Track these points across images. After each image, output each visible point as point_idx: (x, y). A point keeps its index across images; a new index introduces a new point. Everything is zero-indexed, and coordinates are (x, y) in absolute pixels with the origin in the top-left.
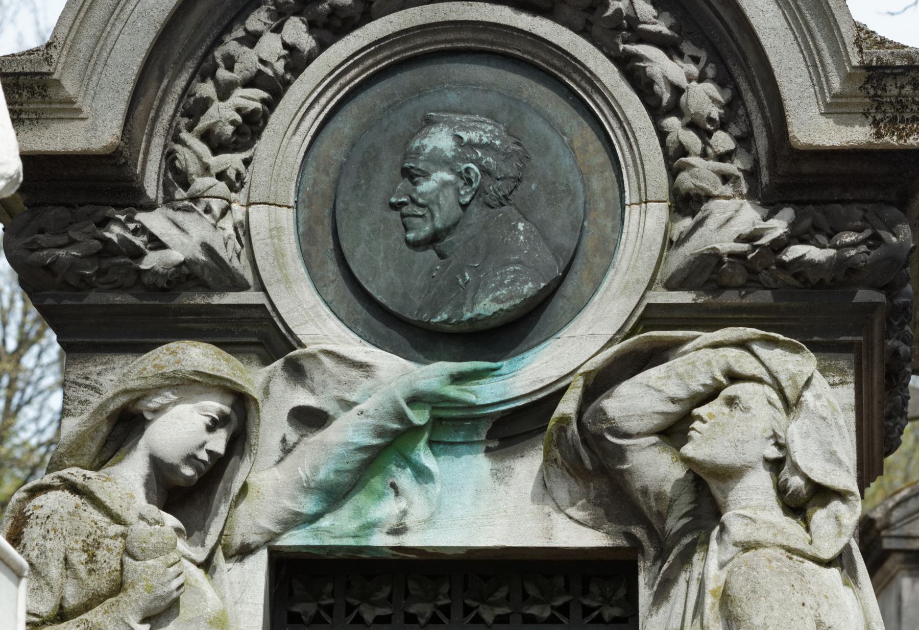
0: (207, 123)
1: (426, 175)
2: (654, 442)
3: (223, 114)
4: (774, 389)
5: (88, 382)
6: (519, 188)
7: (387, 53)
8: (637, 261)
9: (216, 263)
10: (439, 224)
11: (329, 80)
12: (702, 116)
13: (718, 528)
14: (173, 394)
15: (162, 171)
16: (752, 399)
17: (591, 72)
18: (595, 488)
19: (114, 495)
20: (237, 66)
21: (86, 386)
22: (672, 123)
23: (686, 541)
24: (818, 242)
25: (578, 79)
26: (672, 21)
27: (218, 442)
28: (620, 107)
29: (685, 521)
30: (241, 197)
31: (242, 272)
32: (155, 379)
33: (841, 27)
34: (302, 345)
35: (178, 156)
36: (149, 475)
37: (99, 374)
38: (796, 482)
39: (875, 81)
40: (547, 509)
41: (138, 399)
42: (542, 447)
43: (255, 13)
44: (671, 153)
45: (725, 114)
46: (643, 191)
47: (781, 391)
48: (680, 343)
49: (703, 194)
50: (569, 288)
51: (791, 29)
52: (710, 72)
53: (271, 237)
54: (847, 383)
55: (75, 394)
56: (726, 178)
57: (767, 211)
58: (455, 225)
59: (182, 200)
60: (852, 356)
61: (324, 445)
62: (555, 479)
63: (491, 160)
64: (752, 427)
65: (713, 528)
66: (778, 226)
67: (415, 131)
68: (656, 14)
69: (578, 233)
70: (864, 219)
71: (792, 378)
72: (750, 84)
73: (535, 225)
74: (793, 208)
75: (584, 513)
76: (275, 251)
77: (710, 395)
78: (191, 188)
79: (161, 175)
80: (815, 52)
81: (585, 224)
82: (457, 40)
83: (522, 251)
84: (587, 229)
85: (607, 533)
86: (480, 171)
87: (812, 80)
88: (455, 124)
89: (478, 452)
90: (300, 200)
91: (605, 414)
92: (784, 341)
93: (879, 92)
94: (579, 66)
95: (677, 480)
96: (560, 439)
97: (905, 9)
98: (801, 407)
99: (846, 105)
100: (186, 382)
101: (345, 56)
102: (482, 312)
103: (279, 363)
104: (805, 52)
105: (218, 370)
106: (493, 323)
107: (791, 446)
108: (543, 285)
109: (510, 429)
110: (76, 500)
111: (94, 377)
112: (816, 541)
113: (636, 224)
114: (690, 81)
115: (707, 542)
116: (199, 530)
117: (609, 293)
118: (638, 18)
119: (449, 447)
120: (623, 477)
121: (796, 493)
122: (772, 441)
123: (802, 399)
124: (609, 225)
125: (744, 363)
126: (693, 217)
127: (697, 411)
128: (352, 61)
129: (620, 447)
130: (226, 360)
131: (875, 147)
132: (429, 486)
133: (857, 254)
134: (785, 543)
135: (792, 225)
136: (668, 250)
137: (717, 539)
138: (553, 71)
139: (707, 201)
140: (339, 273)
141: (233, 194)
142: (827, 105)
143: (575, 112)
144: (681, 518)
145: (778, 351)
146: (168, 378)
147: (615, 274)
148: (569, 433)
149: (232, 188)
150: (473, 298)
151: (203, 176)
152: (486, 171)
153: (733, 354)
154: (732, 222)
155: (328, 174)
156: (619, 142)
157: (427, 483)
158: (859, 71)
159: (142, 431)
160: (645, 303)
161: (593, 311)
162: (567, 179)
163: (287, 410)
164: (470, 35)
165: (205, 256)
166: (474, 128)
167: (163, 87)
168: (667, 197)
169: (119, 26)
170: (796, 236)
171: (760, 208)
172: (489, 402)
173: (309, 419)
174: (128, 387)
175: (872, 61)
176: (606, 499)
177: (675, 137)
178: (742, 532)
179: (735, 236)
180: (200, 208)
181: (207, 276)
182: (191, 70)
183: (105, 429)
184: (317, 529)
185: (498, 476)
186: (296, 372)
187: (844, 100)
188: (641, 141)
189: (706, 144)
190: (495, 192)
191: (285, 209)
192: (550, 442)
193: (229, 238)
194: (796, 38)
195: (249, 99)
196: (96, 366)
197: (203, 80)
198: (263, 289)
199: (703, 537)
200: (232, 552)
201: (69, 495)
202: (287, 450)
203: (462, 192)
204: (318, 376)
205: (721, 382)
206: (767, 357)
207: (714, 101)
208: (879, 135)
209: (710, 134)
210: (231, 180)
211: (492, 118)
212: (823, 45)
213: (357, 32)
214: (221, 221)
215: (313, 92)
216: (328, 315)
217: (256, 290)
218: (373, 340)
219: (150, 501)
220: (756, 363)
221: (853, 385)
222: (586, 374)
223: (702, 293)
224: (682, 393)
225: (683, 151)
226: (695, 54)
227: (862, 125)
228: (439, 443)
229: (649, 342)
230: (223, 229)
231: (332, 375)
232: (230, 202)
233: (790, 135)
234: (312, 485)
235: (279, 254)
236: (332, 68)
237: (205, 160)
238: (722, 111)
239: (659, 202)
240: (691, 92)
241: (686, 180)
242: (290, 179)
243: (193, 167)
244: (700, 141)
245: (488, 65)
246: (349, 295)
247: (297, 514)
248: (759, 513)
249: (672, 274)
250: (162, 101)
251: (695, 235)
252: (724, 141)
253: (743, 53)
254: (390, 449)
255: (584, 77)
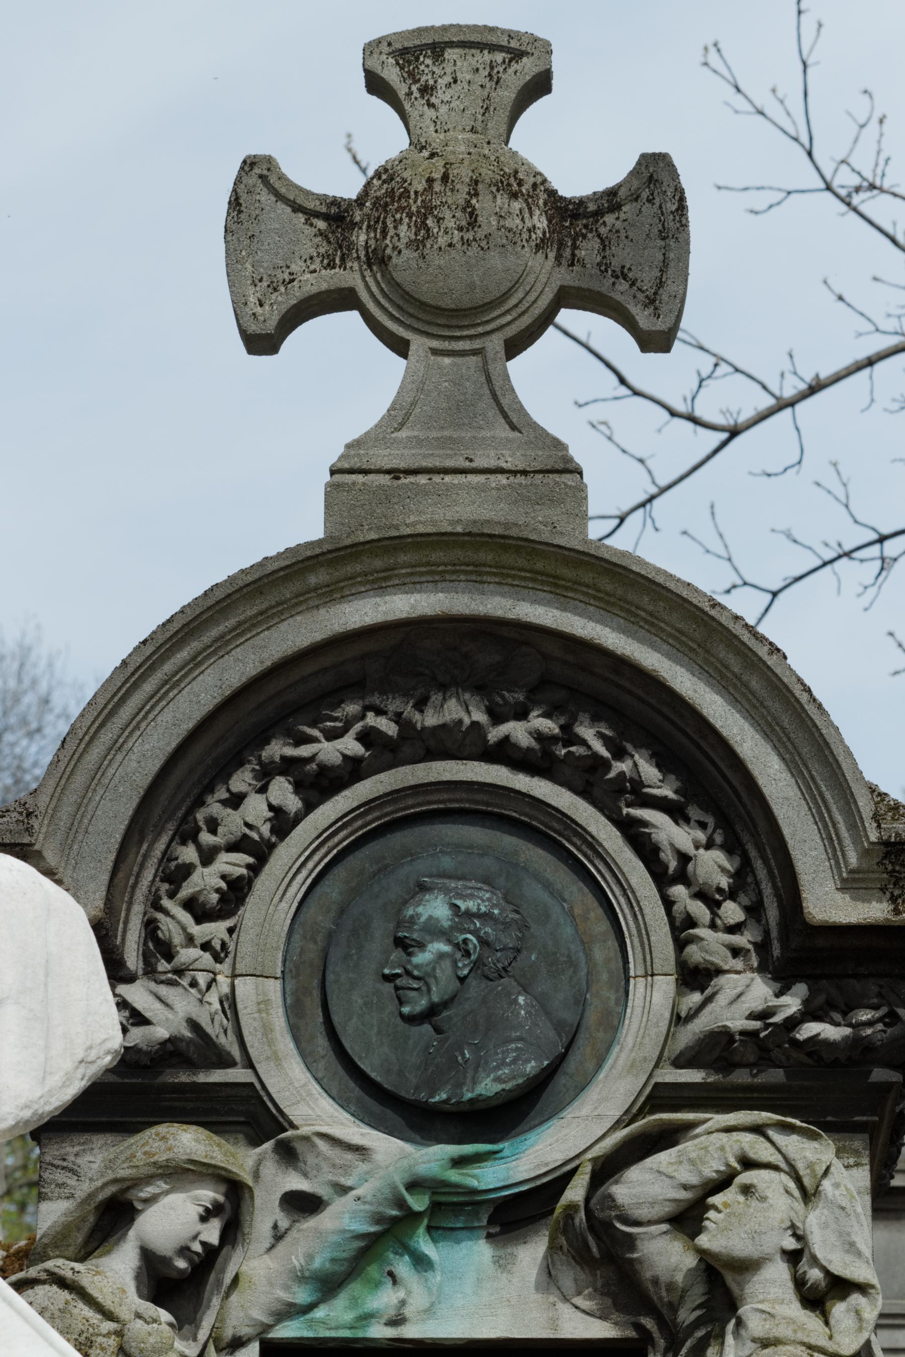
0: (191, 891)
1: (421, 946)
2: (665, 1230)
3: (207, 881)
4: (791, 1177)
5: (65, 1164)
6: (518, 959)
7: (376, 814)
8: (643, 1037)
9: (202, 1039)
10: (436, 999)
11: (317, 843)
12: (711, 886)
13: (733, 1321)
14: (166, 1183)
15: (142, 940)
16: (769, 1187)
17: (593, 837)
18: (602, 1277)
19: (105, 1290)
20: (220, 830)
21: (63, 1168)
22: (679, 891)
23: (700, 1333)
24: (832, 1018)
25: (579, 843)
26: (677, 784)
27: (212, 1233)
28: (623, 874)
29: (698, 1313)
30: (225, 968)
31: (229, 1049)
32: (147, 1168)
33: (858, 800)
34: (293, 1126)
35: (161, 926)
36: (140, 1268)
37: (76, 1155)
38: (815, 1275)
39: (893, 857)
40: (552, 1299)
41: (128, 1188)
42: (547, 1233)
43: (239, 772)
44: (678, 924)
45: (734, 883)
46: (649, 963)
47: (798, 1180)
48: (691, 1126)
49: (713, 968)
50: (571, 1065)
51: (805, 799)
52: (718, 839)
53: (259, 1011)
54: (862, 1165)
55: (51, 1176)
56: (736, 952)
57: (778, 985)
58: (453, 999)
59: (165, 973)
60: (866, 1136)
61: (318, 1233)
62: (560, 1267)
63: (490, 931)
64: (769, 1217)
65: (729, 1321)
66: (791, 1004)
67: (407, 897)
68: (661, 778)
69: (581, 1008)
70: (880, 995)
71: (810, 1166)
72: (759, 851)
73: (535, 998)
74: (807, 984)
75: (591, 1303)
76: (264, 1025)
77: (723, 1183)
78: (176, 960)
79: (141, 945)
80: (830, 825)
81: (588, 996)
82: (450, 801)
83: (524, 1027)
84: (589, 1002)
85: (616, 1324)
86: (479, 942)
87: (827, 854)
88: (451, 891)
89: (478, 1238)
90: (287, 970)
91: (614, 1200)
92: (801, 1127)
93: (897, 868)
94: (580, 830)
95: (689, 1270)
96: (567, 1225)
97: (786, 470)
98: (820, 1196)
99: (863, 880)
100: (179, 1171)
101: (333, 818)
102: (483, 1092)
103: (268, 1145)
104: (819, 824)
105: (212, 1158)
106: (494, 1103)
107: (809, 1237)
108: (546, 1063)
109: (512, 1215)
110: (65, 1295)
111: (71, 1158)
112: (837, 1337)
113: (642, 998)
114: (697, 848)
115: (721, 1336)
116: (190, 1324)
117: (614, 1071)
118: (642, 781)
119: (448, 1233)
120: (633, 1266)
121: (815, 1286)
122: (790, 1232)
123: (821, 1188)
124: (613, 997)
125: (761, 1150)
126: (702, 992)
127: (711, 1200)
128: (340, 823)
129: (630, 1236)
130: (219, 1145)
131: (893, 924)
132: (429, 1275)
133: (874, 1033)
134: (806, 1340)
135: (806, 1002)
136: (676, 1025)
137: (733, 1333)
138: (552, 834)
139: (717, 976)
140: (330, 1049)
141: (218, 965)
142: (843, 880)
143: (575, 877)
144: (694, 1310)
145: (795, 1137)
146: (161, 1167)
147: (621, 1050)
148: (577, 1221)
149: (218, 959)
150: (473, 1078)
151: (187, 946)
152: (484, 942)
153: (748, 1139)
154: (743, 998)
155: (316, 942)
156: (622, 910)
157: (426, 1271)
158: (877, 847)
159: (132, 1221)
160: (653, 1082)
161: (598, 1090)
162: (569, 949)
163: (278, 1195)
164: (464, 795)
165: (191, 1032)
166: (471, 897)
167: (142, 851)
168: (674, 970)
169: (100, 791)
170: (810, 1013)
171: (771, 982)
172: (491, 1187)
173: (302, 1204)
174: (119, 1176)
175: (890, 836)
176: (613, 1288)
177: (682, 908)
178: (760, 1328)
179: (747, 1013)
180: (185, 982)
181: (192, 1053)
182: (171, 833)
183: (92, 1219)
184: (312, 1320)
185: (502, 1264)
186: (288, 1154)
187: (861, 876)
188: (646, 911)
189: (714, 914)
190: (494, 964)
191: (273, 980)
192: (557, 1230)
193: (216, 1013)
194: (810, 809)
195: (235, 865)
196: (73, 1146)
197: (184, 843)
198: (250, 1064)
199: (717, 1329)
200: (223, 1344)
201: (58, 1290)
202: (278, 1236)
203: (460, 965)
204: (311, 1160)
205: (735, 1168)
206: (783, 1144)
207: (723, 870)
208: (897, 912)
209: (719, 904)
210: (216, 951)
211: (489, 884)
212: (839, 818)
213: (346, 793)
214: (207, 994)
215: (300, 856)
216: (319, 1094)
217: (244, 1068)
218: (367, 1120)
219: (141, 1296)
220: (772, 1150)
221: (868, 1167)
222: (594, 1160)
223: (712, 1071)
224: (694, 1180)
225: (690, 922)
226: (702, 819)
227: (880, 901)
228: (438, 1228)
229: (658, 1125)
230: (210, 1004)
231: (326, 1159)
232: (215, 974)
233: (806, 911)
234: (307, 1274)
235: (267, 1029)
236: (320, 831)
237: (190, 930)
238: (731, 881)
239: (666, 975)
240: (699, 862)
241: (694, 953)
242: (277, 948)
243: (177, 939)
244: (708, 912)
245: (483, 826)
246: (341, 1072)
247: (291, 1305)
248: (777, 1307)
249: (681, 1051)
250: (142, 866)
251: (704, 1011)
252: (734, 912)
253: (752, 820)
254: (389, 1235)
255: (585, 841)
